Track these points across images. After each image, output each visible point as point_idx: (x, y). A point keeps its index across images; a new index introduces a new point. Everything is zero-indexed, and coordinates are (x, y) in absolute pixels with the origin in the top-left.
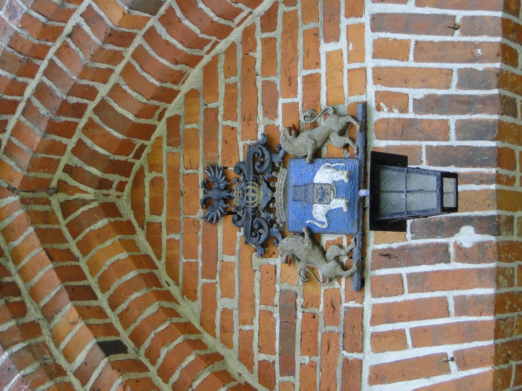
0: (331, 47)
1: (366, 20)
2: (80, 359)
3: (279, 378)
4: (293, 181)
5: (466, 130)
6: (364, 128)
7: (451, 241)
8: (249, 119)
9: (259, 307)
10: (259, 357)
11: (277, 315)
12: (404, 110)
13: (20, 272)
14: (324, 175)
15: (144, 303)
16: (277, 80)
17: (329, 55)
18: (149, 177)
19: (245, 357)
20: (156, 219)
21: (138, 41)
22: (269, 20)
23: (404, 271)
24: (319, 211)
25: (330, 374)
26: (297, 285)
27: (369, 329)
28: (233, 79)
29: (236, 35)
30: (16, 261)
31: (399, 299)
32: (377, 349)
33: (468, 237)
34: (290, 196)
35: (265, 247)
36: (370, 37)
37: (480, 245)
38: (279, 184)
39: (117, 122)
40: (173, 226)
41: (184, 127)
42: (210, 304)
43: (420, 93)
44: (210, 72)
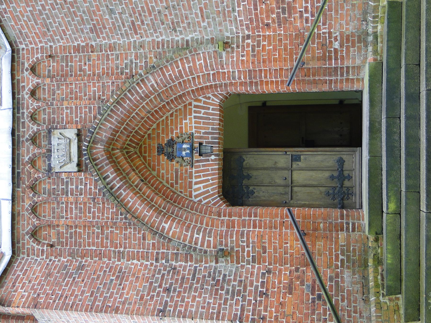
0: (185, 121)
1: (193, 117)
2: (136, 183)
3: (175, 185)
4: (178, 147)
5: (212, 138)
6: (193, 137)
7: (210, 158)
8: (167, 135)
9: (170, 172)
10: (170, 182)
11: (174, 173)
12: (200, 134)
13: (120, 166)
14: (185, 146)
15: (146, 172)
16: (174, 127)
17: (185, 123)
18: (143, 146)
19: (167, 182)
20: (145, 155)
21: (145, 119)
22: (172, 115)
23: (201, 164)
24: (184, 153)
25: (186, 184)
26: (179, 167)
27: (194, 175)
28: (163, 126)
29: (164, 118)
30: (119, 164)
31: (200, 169)
32: (196, 178)
33: (213, 157)
34: (177, 150)
35: (172, 160)
36: (193, 120)
37: (215, 159)
38: (175, 148)
39: (140, 135)
40: (149, 156)
41: (152, 136)
42: (159, 172)
43: (204, 131)
44: (158, 125)
